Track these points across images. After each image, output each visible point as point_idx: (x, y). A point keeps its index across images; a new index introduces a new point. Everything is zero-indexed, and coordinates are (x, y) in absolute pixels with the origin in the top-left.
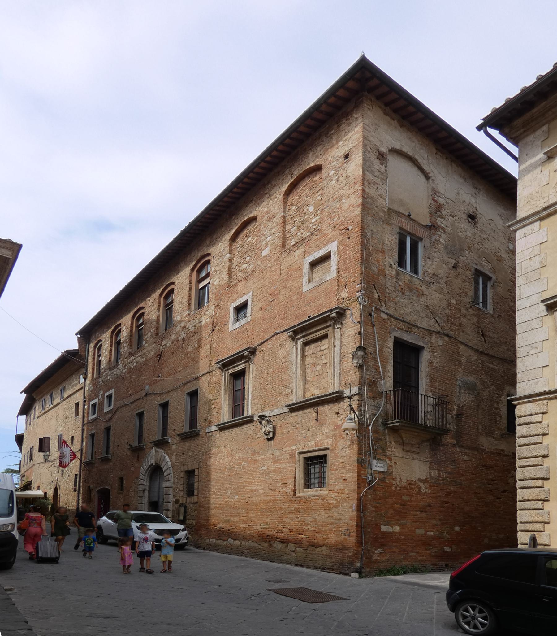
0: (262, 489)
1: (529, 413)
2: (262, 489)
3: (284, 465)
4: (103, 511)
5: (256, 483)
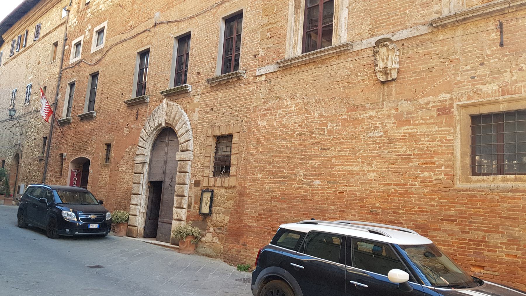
0: (374, 171)
2: (374, 171)
5: (359, 160)
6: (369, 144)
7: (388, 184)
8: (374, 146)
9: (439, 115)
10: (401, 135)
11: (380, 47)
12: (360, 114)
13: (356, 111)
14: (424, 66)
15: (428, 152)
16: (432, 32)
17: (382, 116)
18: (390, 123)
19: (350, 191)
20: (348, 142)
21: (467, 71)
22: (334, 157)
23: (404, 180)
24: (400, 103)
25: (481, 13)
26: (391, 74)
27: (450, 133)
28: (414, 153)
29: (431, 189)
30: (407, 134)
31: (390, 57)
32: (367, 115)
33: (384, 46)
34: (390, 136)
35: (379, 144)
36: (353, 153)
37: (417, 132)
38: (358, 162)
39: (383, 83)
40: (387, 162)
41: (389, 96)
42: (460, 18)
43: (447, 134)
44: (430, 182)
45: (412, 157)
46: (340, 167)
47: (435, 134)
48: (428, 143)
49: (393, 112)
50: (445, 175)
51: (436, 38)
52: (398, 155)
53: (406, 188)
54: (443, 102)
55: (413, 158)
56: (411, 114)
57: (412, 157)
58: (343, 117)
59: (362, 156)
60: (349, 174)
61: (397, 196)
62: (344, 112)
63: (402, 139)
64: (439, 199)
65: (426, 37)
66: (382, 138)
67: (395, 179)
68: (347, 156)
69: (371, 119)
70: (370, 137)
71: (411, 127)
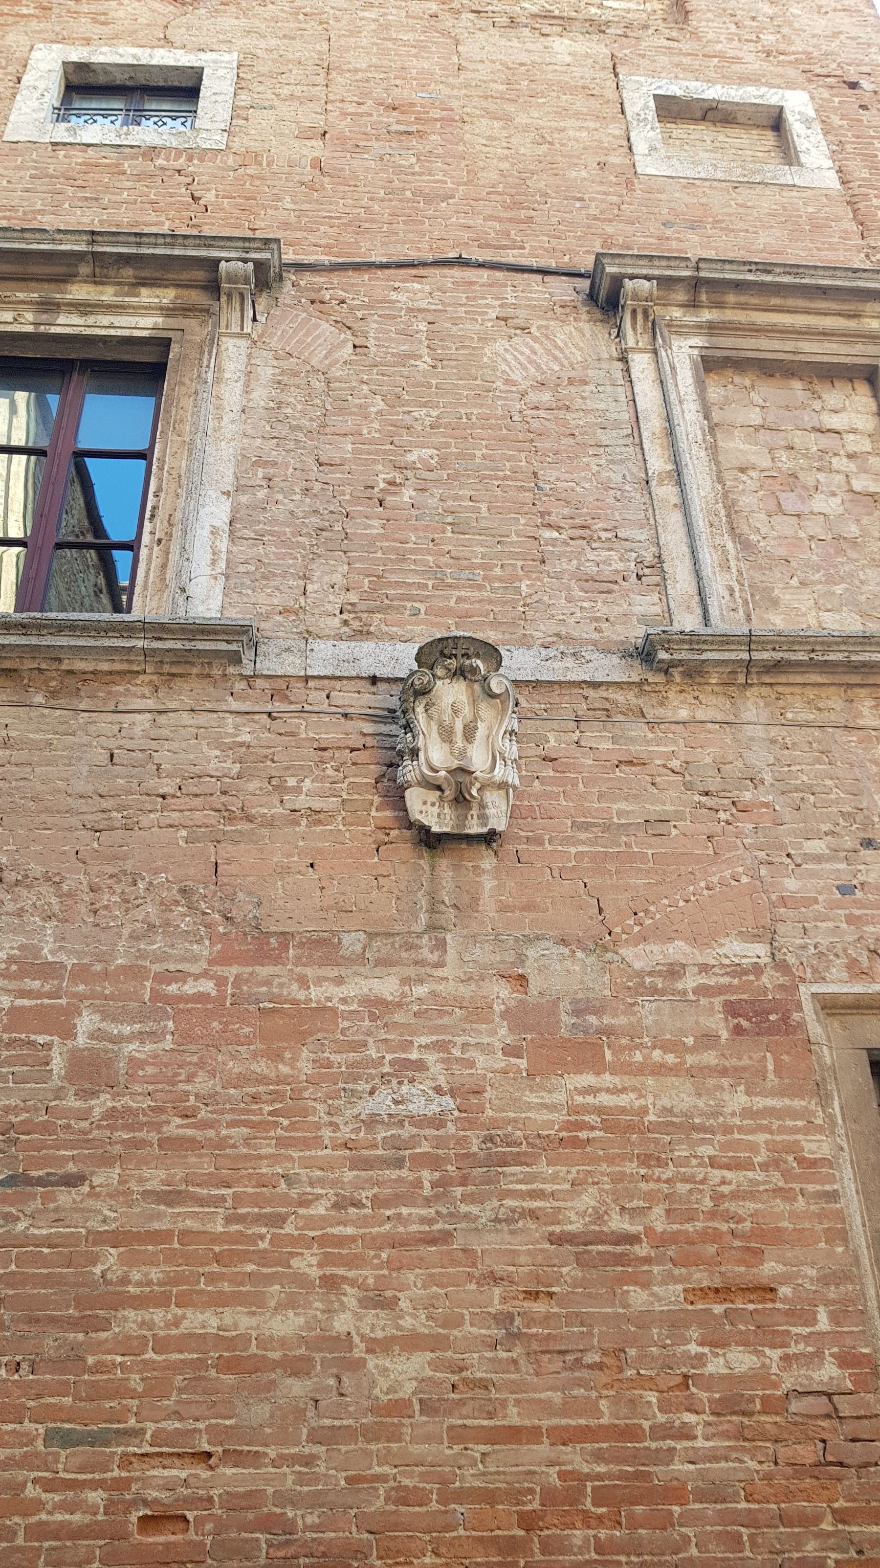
0: (412, 1342)
1: (657, 385)
2: (412, 1342)
3: (681, 1096)
4: (83, 1360)
5: (307, 1263)
6: (367, 1164)
7: (514, 1435)
8: (404, 1173)
9: (738, 1030)
10: (561, 1117)
11: (439, 672)
12: (303, 982)
13: (277, 960)
14: (623, 806)
15: (724, 1227)
16: (640, 684)
17: (440, 1005)
18: (487, 1049)
19: (237, 1503)
20: (222, 1143)
21: (818, 859)
22: (116, 1239)
23: (615, 1401)
24: (531, 953)
25: (839, 656)
26: (482, 806)
27: (810, 1127)
28: (649, 1231)
29: (783, 1452)
30: (592, 1119)
31: (482, 730)
32: (350, 990)
33: (461, 673)
34: (494, 1124)
35: (433, 1162)
36: (259, 1219)
37: (644, 1111)
38: (300, 1279)
39: (429, 841)
40: (494, 1279)
41: (467, 907)
42: (766, 655)
43: (796, 1130)
44: (769, 1406)
45: (642, 1250)
46: (158, 1316)
47: (740, 1129)
48: (716, 1175)
49: (502, 993)
50: (845, 1361)
51: (660, 712)
52: (556, 1240)
53: (634, 1457)
54: (746, 972)
55: (647, 1260)
56: (598, 1012)
57: (642, 1250)
58: (190, 988)
59: (323, 1241)
60: (227, 1366)
61: (587, 1519)
62: (195, 959)
63: (568, 1142)
64: (841, 1516)
65: (619, 697)
66: (451, 1128)
67: (556, 1397)
68: (216, 1238)
69: (373, 1017)
70: (372, 1122)
71: (608, 1080)
